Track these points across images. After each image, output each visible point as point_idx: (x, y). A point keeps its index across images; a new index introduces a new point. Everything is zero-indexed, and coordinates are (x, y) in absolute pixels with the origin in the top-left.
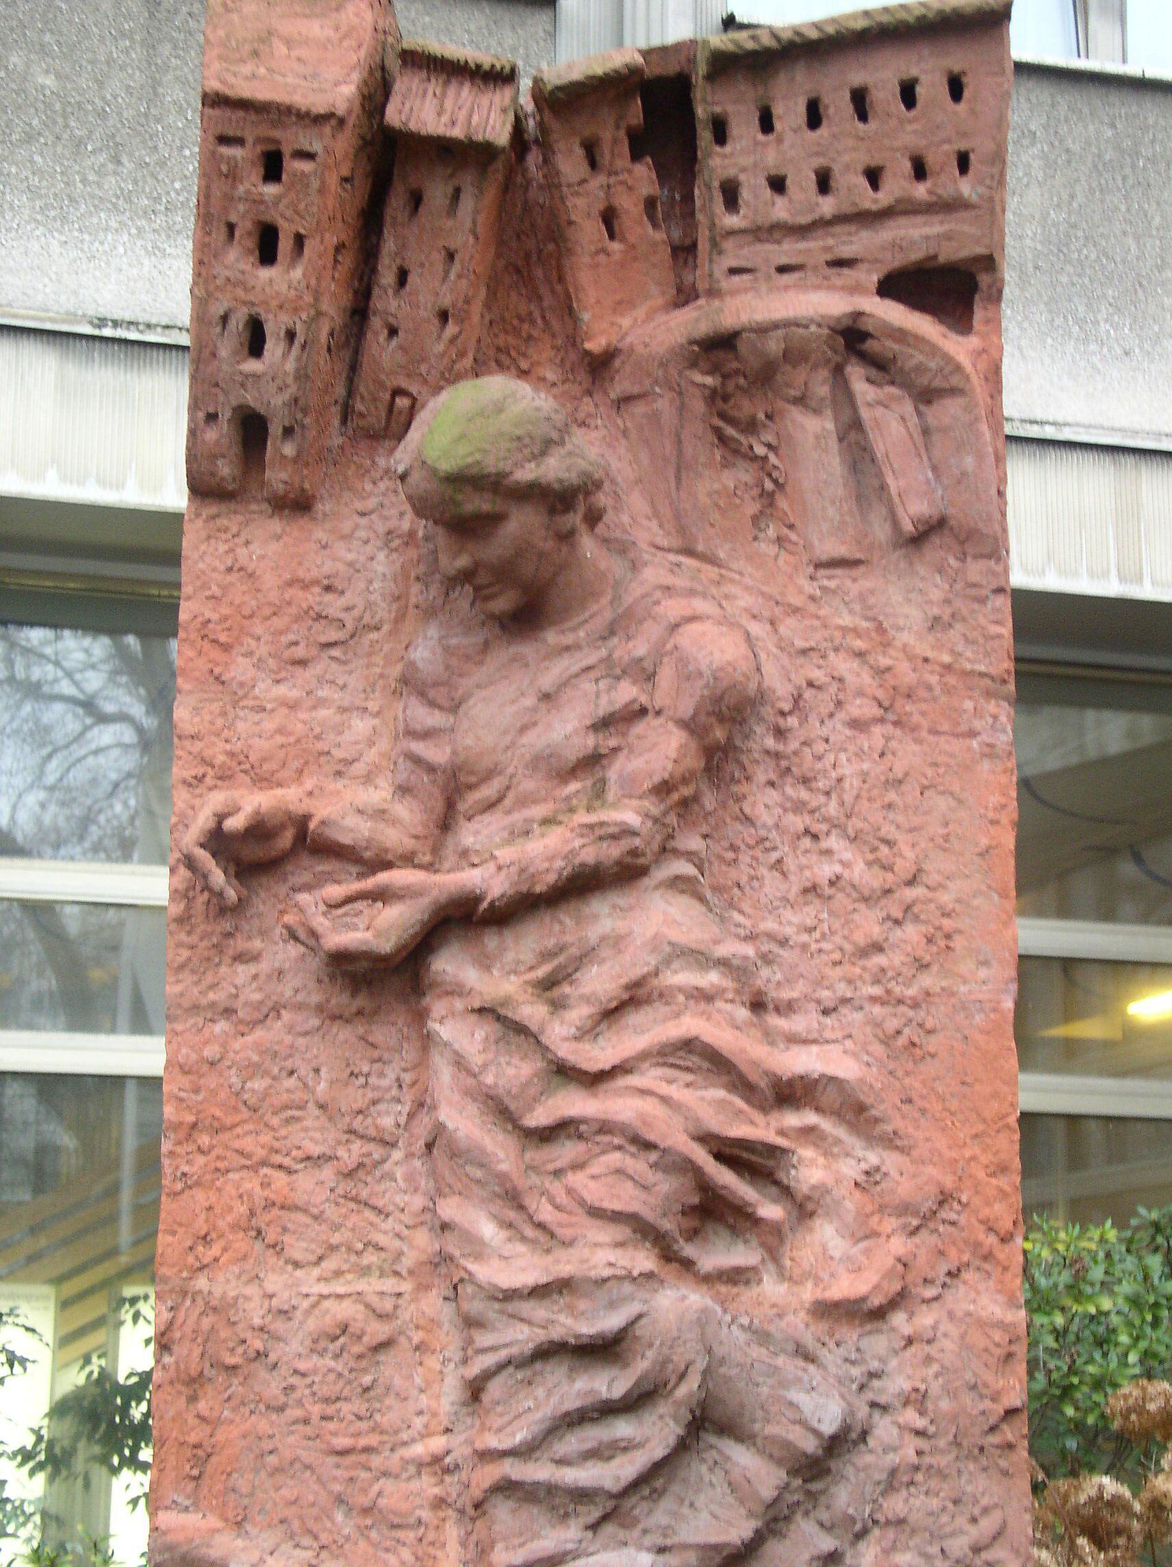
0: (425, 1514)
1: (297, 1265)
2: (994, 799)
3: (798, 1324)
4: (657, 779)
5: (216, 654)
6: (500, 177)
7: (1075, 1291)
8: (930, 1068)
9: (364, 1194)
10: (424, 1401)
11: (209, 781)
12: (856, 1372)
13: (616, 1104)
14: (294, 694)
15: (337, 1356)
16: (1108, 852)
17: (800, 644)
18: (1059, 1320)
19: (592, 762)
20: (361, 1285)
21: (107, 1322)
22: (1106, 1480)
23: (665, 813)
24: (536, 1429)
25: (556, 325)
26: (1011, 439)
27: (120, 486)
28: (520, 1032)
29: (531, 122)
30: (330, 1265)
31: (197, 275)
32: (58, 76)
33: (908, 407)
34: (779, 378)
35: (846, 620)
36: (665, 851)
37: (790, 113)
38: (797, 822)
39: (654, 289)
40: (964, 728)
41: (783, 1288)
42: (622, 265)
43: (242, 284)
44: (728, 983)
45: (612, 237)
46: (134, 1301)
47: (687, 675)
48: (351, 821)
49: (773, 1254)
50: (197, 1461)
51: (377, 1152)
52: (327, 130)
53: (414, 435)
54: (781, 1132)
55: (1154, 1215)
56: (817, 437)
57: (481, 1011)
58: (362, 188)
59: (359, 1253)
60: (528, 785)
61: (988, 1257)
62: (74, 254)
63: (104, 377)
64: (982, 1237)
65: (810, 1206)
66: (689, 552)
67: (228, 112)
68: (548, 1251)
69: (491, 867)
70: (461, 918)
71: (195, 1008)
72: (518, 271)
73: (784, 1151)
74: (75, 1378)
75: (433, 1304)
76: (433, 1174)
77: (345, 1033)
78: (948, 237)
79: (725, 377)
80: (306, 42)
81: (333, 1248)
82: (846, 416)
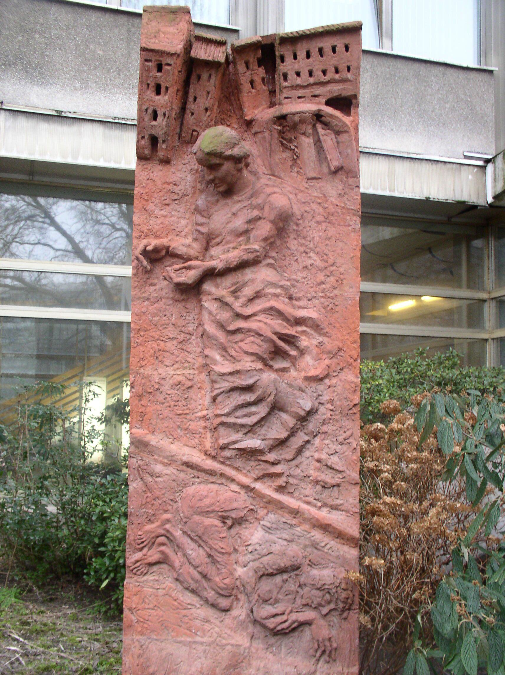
0: (202, 431)
1: (167, 366)
2: (355, 243)
3: (300, 382)
4: (264, 237)
5: (144, 202)
6: (222, 71)
7: (373, 378)
8: (336, 315)
9: (185, 348)
10: (201, 402)
11: (142, 237)
12: (315, 395)
13: (252, 324)
14: (165, 213)
15: (178, 390)
16: (385, 265)
17: (303, 200)
18: (369, 386)
19: (246, 232)
20: (184, 372)
21: (120, 387)
22: (379, 424)
23: (266, 246)
24: (231, 409)
25: (237, 112)
26: (361, 152)
27: (120, 163)
28: (225, 305)
29: (231, 57)
30: (176, 366)
31: (139, 98)
32: (103, 51)
33: (333, 136)
34: (298, 127)
35: (316, 194)
36: (266, 256)
37: (302, 54)
38: (302, 249)
39: (264, 103)
40: (347, 224)
41: (296, 373)
42: (255, 96)
43: (151, 100)
44: (283, 292)
45: (253, 88)
46: (126, 381)
47: (272, 208)
48: (181, 248)
49: (294, 364)
50: (141, 416)
51: (188, 337)
52: (175, 58)
53: (198, 142)
54: (296, 332)
55: (394, 359)
56: (308, 144)
57: (216, 299)
58: (184, 74)
59: (183, 363)
60: (229, 238)
61: (350, 365)
62: (108, 100)
63: (116, 133)
64: (349, 360)
65: (304, 352)
66: (273, 175)
67: (147, 53)
68: (234, 363)
69: (219, 260)
70: (210, 274)
71: (139, 298)
72: (227, 98)
73: (297, 337)
74: (112, 401)
75: (203, 376)
76: (203, 342)
77: (179, 305)
78: (344, 89)
79: (283, 127)
80: (169, 33)
81: (176, 362)
82: (316, 138)
